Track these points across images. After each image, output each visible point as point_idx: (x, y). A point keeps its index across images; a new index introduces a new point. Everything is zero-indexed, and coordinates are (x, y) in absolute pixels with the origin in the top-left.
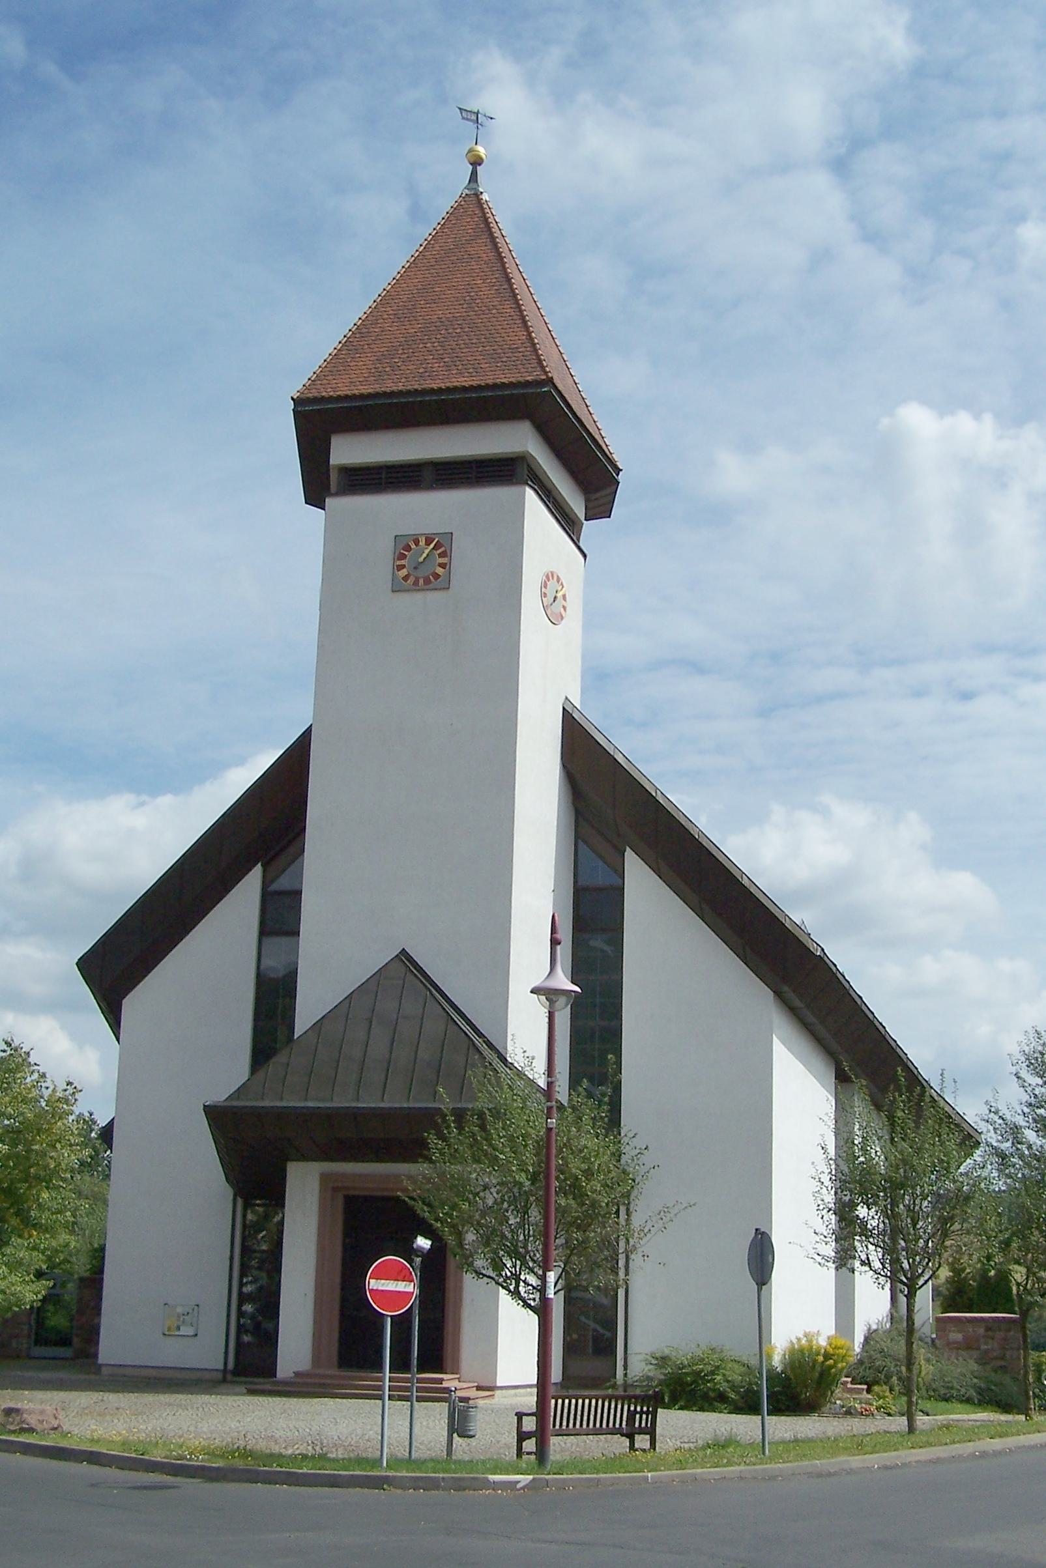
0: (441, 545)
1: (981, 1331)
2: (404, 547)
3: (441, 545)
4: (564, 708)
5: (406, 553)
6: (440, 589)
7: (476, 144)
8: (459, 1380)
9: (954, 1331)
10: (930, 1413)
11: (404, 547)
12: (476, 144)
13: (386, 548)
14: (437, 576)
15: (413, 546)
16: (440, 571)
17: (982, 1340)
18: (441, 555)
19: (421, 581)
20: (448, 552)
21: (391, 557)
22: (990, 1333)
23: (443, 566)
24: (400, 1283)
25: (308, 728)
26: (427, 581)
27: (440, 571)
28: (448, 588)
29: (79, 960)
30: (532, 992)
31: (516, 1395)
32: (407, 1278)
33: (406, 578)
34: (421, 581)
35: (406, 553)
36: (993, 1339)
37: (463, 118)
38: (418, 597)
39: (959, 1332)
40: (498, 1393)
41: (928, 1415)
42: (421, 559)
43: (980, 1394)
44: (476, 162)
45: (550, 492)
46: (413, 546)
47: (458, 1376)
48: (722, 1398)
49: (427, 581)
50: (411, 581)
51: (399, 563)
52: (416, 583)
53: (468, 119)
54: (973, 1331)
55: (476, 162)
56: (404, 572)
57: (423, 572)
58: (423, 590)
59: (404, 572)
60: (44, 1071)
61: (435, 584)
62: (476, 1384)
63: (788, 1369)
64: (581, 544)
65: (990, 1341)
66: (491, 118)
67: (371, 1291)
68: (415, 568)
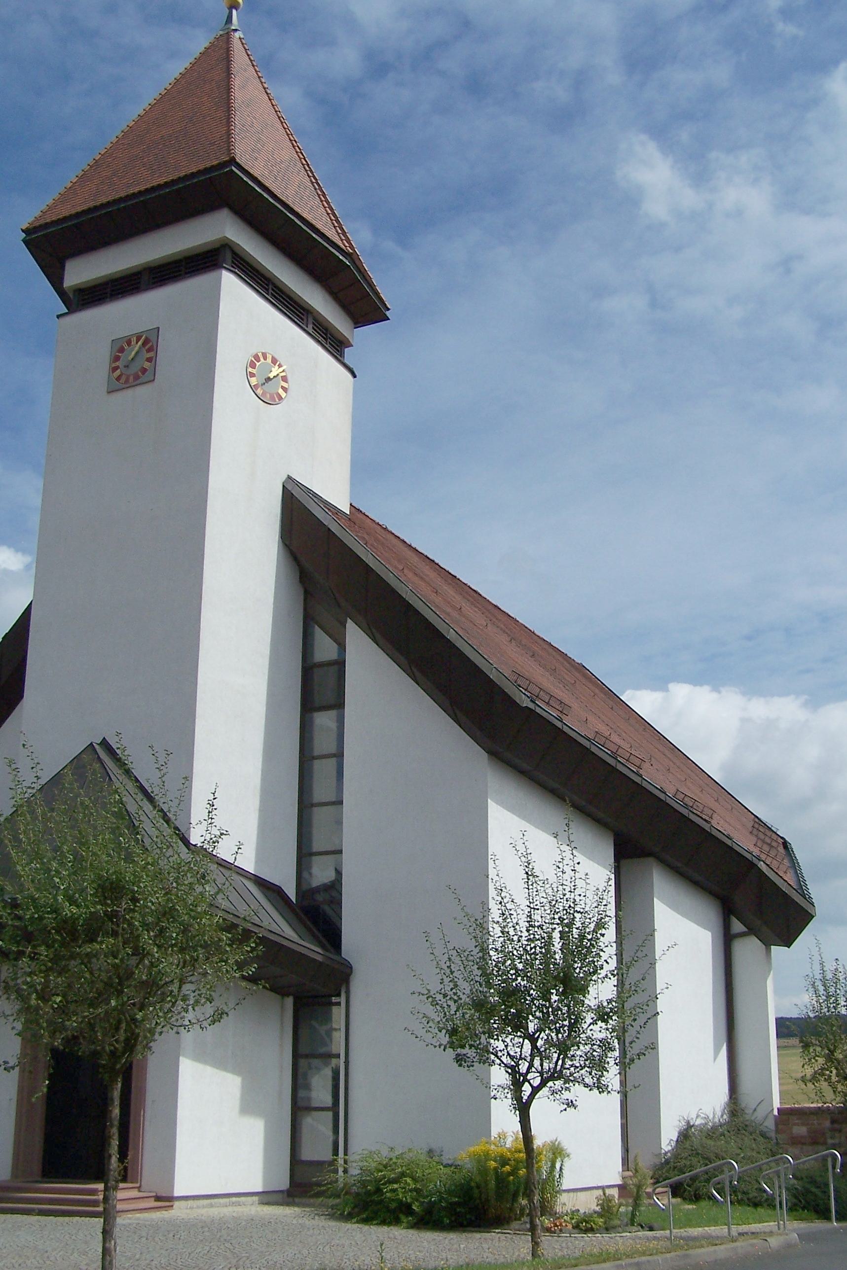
1: (827, 1124)
4: (284, 486)
5: (120, 355)
6: (146, 383)
8: (139, 1189)
9: (797, 1124)
10: (655, 1225)
13: (104, 353)
14: (144, 371)
16: (147, 365)
17: (828, 1134)
18: (149, 351)
20: (155, 347)
22: (836, 1126)
23: (149, 360)
26: (137, 377)
27: (147, 365)
28: (154, 380)
31: (211, 1206)
33: (118, 379)
35: (120, 355)
36: (840, 1131)
38: (129, 393)
39: (803, 1124)
40: (177, 1204)
41: (651, 1229)
43: (796, 1197)
45: (326, 329)
47: (138, 1185)
48: (406, 1209)
50: (123, 380)
51: (114, 365)
52: (127, 381)
54: (819, 1124)
56: (118, 372)
57: (135, 368)
58: (134, 386)
59: (118, 372)
61: (144, 378)
62: (154, 1194)
63: (475, 1169)
64: (346, 361)
65: (837, 1135)
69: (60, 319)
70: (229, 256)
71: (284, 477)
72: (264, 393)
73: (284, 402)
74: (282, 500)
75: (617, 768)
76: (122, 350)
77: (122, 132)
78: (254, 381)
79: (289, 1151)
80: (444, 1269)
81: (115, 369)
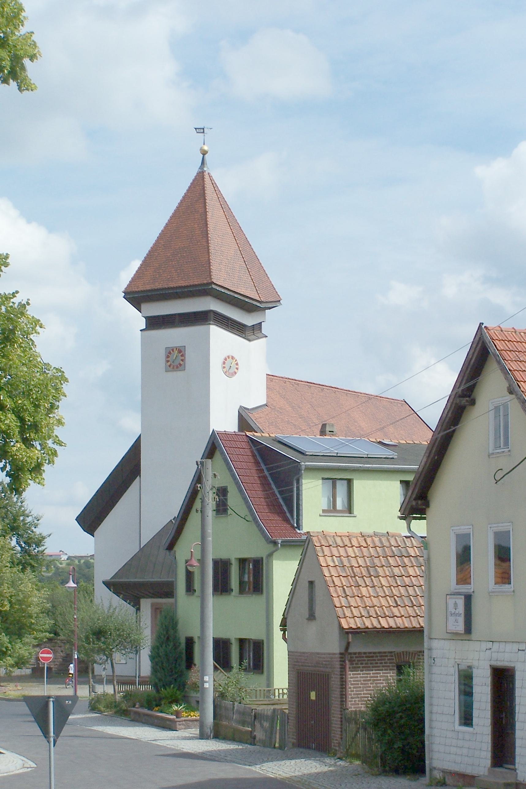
0: (181, 351)
2: (169, 352)
3: (181, 351)
7: (204, 144)
11: (169, 352)
12: (204, 144)
14: (180, 365)
15: (172, 352)
16: (181, 362)
19: (175, 367)
21: (164, 358)
23: (182, 360)
24: (474, 683)
25: (138, 438)
26: (177, 367)
27: (181, 362)
29: (84, 531)
30: (104, 583)
32: (50, 653)
33: (170, 366)
34: (175, 367)
37: (197, 132)
42: (174, 358)
44: (204, 153)
46: (172, 352)
49: (177, 367)
50: (172, 367)
51: (167, 359)
53: (199, 133)
55: (204, 153)
56: (169, 363)
57: (176, 363)
59: (169, 363)
60: (6, 253)
61: (180, 368)
66: (211, 129)
67: (41, 657)
68: (173, 362)
69: (317, 614)
70: (212, 315)
71: (238, 407)
72: (229, 374)
73: (237, 374)
74: (239, 418)
75: (66, 725)
76: (170, 353)
77: (225, 431)
78: (225, 370)
79: (104, 521)
80: (3, 53)
81: (168, 361)
